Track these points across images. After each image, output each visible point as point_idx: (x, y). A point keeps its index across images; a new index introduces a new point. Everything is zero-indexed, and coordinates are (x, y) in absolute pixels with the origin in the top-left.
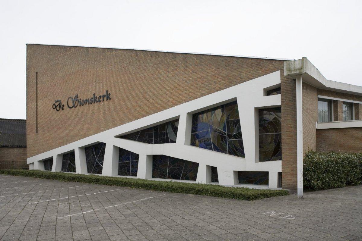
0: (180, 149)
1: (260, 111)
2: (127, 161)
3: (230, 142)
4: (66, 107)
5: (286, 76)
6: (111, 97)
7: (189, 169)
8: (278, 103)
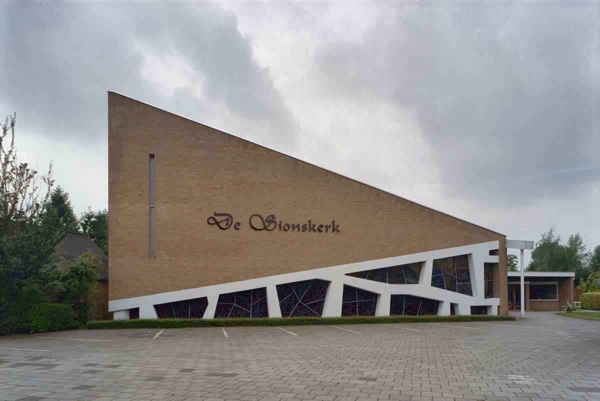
0: (424, 289)
3: (459, 285)
7: (432, 306)
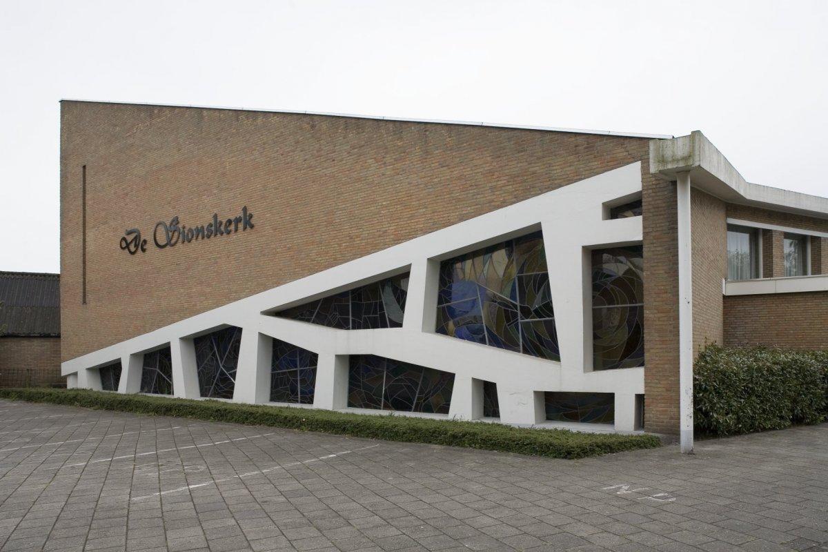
0: (411, 340)
1: (595, 255)
2: (290, 368)
3: (526, 325)
4: (150, 246)
5: (654, 175)
6: (253, 221)
7: (431, 387)
8: (637, 236)
